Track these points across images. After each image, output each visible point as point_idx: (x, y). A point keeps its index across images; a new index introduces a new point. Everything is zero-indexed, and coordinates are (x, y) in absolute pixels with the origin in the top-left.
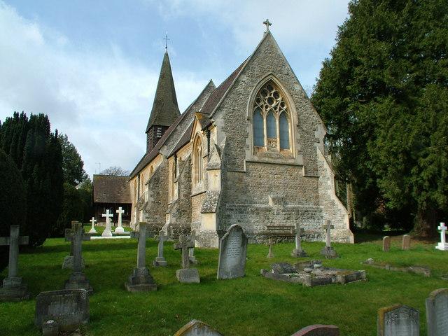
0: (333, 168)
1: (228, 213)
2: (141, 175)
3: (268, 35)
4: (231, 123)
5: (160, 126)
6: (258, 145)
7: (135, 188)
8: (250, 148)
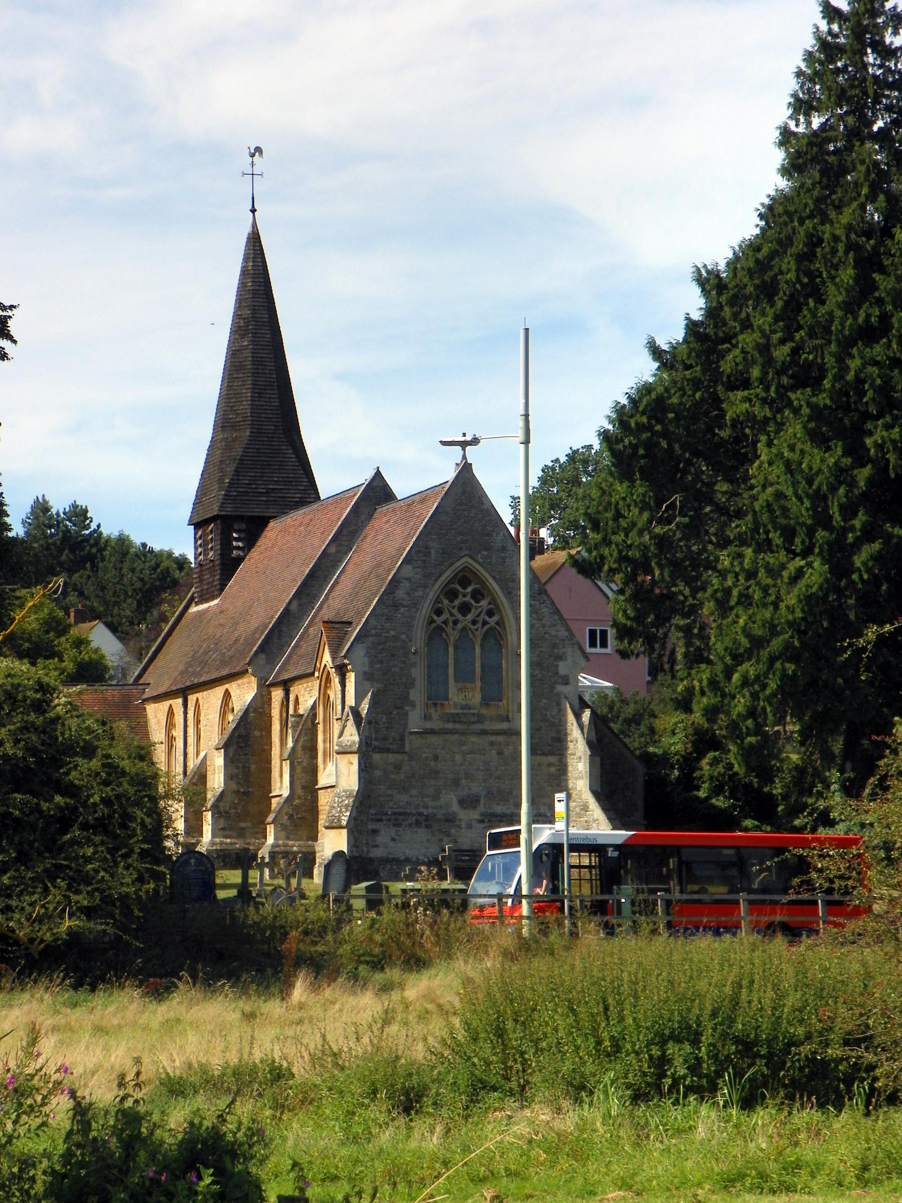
0: (590, 743)
1: (371, 826)
2: (192, 699)
3: (466, 470)
4: (381, 662)
5: (240, 518)
6: (436, 698)
7: (171, 740)
8: (418, 706)
